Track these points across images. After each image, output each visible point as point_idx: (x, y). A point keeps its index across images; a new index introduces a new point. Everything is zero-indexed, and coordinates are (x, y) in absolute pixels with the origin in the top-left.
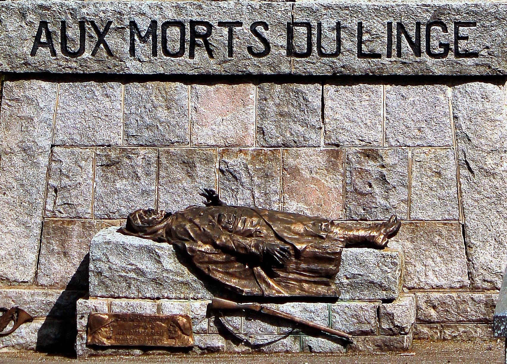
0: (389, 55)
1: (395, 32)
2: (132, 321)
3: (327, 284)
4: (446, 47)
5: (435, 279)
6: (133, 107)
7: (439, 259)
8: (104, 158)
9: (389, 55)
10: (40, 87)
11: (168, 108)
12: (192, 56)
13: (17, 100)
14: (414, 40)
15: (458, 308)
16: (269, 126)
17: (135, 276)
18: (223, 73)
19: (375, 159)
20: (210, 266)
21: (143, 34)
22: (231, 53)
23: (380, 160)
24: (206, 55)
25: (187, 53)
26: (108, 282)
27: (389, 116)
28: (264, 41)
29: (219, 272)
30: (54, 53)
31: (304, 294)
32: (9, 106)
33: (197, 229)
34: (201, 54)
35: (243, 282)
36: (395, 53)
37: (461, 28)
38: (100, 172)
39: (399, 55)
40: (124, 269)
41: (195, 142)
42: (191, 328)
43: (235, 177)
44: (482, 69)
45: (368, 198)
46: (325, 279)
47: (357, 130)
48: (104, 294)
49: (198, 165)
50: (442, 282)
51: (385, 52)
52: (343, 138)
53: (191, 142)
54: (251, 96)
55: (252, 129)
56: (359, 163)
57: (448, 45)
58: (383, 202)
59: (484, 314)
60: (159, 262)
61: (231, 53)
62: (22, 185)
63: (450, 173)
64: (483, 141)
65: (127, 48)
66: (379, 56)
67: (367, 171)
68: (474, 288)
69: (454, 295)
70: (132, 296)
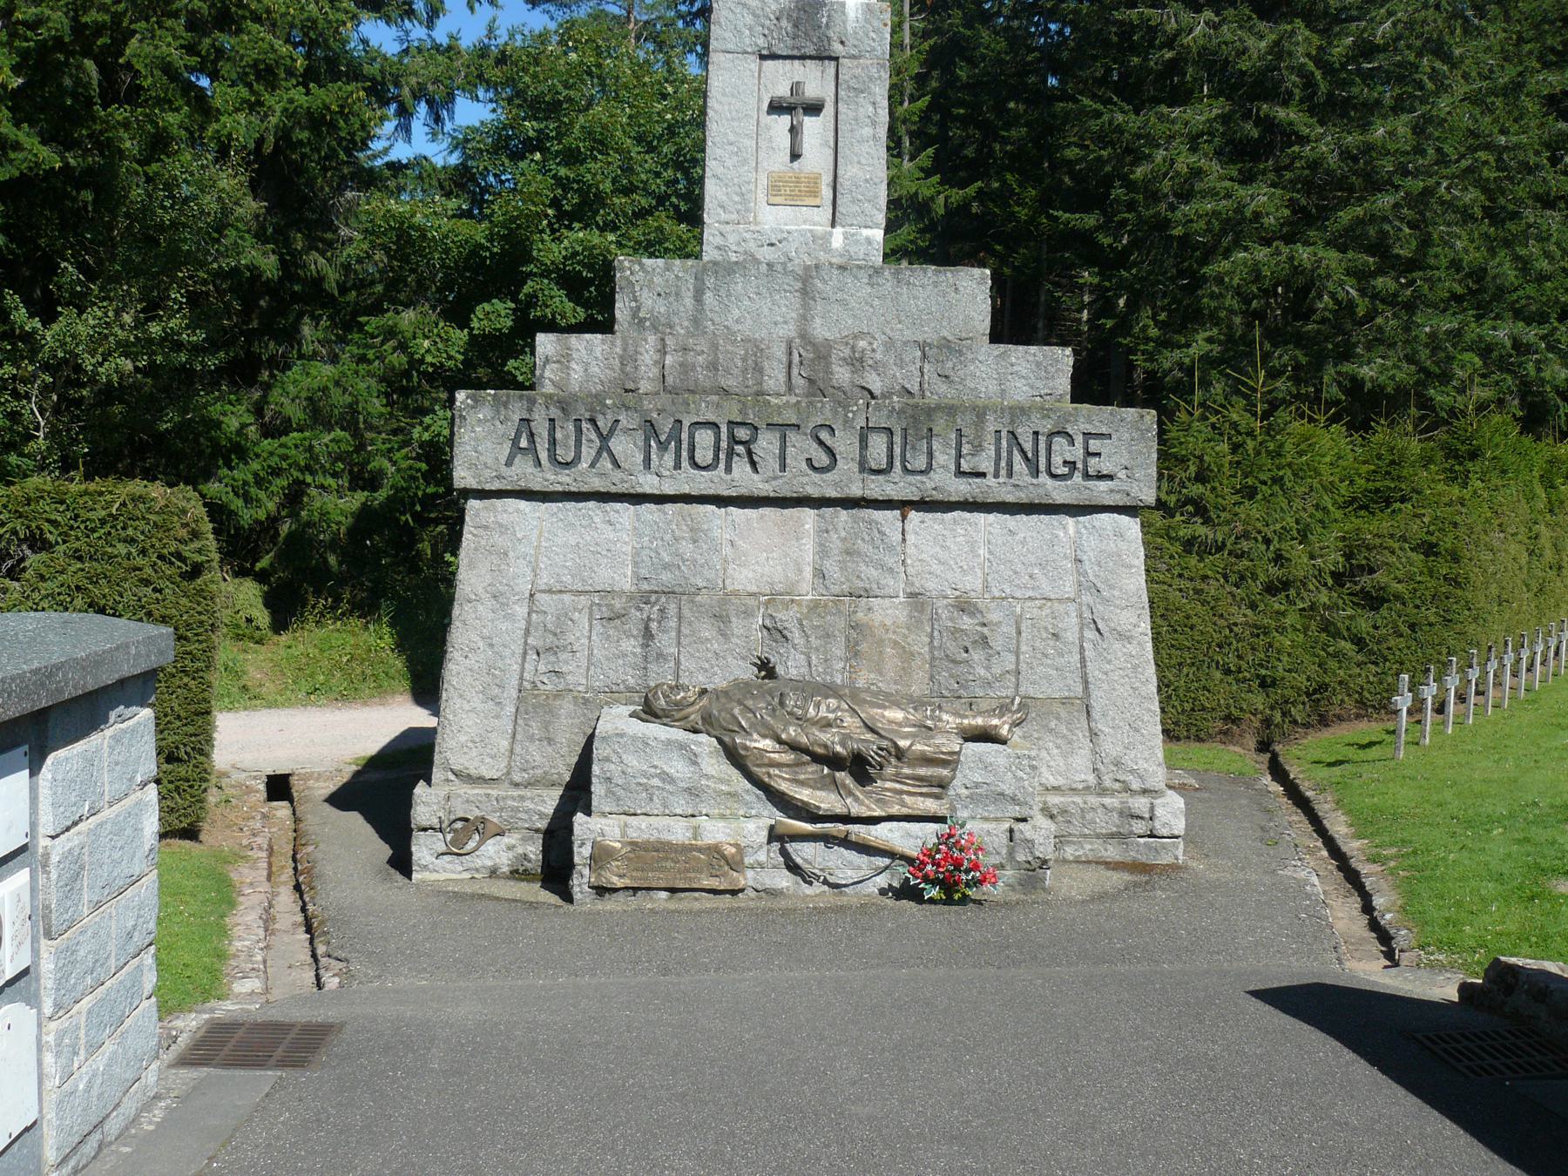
0: (996, 476)
1: (1004, 443)
2: (657, 851)
3: (937, 797)
4: (1071, 465)
5: (1051, 778)
6: (646, 539)
7: (1056, 751)
8: (604, 609)
9: (996, 476)
10: (518, 511)
11: (695, 541)
12: (728, 469)
13: (486, 527)
14: (1016, 452)
15: (1083, 817)
16: (831, 567)
17: (660, 785)
18: (772, 495)
19: (972, 614)
20: (771, 771)
21: (663, 438)
22: (783, 467)
23: (979, 616)
24: (748, 468)
25: (722, 465)
26: (620, 792)
27: (991, 557)
28: (830, 452)
29: (784, 779)
30: (539, 463)
31: (905, 811)
32: (474, 535)
33: (751, 715)
34: (741, 468)
35: (818, 793)
36: (1003, 472)
37: (1091, 442)
38: (598, 627)
39: (1010, 474)
40: (644, 774)
41: (730, 588)
42: (742, 862)
43: (784, 637)
44: (1118, 497)
45: (963, 668)
46: (936, 790)
47: (949, 576)
48: (614, 809)
49: (733, 619)
50: (1061, 781)
51: (992, 470)
52: (932, 585)
53: (724, 588)
54: (807, 526)
55: (808, 572)
56: (952, 619)
57: (1074, 463)
58: (982, 672)
59: (1118, 826)
60: (695, 763)
61: (783, 467)
62: (491, 645)
63: (1071, 636)
64: (1116, 593)
65: (639, 458)
66: (983, 475)
67: (962, 630)
68: (1103, 791)
69: (1078, 800)
70: (656, 812)
